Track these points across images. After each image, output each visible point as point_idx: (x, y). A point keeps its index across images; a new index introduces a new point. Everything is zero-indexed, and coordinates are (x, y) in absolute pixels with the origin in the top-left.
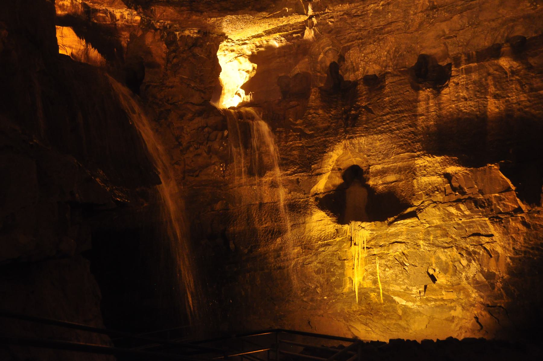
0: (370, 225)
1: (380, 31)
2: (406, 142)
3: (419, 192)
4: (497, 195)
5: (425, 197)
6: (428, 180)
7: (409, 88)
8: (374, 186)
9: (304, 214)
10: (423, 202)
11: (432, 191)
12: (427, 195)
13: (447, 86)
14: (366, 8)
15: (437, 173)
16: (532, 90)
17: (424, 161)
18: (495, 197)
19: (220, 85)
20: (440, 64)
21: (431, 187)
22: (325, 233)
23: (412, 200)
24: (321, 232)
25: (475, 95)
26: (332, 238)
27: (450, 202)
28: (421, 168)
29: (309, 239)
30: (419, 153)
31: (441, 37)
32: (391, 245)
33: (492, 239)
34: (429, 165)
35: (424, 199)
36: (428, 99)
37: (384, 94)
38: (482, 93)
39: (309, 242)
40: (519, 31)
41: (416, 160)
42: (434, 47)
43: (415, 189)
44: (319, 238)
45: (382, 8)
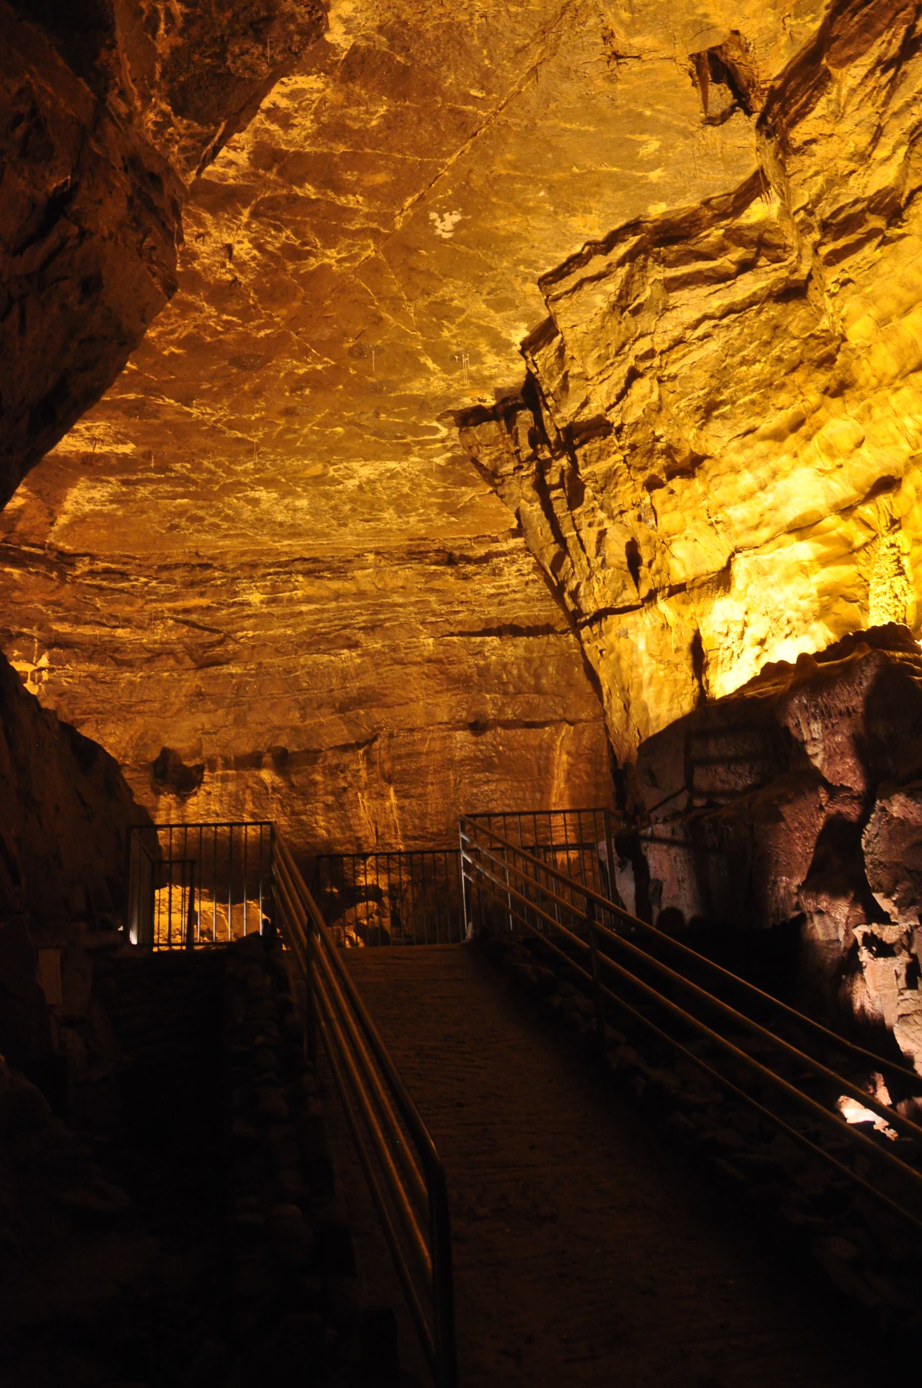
1: (128, 708)
7: (148, 790)
13: (195, 794)
14: (119, 676)
16: (293, 813)
19: (874, 1021)
20: (185, 763)
25: (230, 811)
36: (169, 808)
38: (238, 809)
40: (283, 741)
42: (181, 741)
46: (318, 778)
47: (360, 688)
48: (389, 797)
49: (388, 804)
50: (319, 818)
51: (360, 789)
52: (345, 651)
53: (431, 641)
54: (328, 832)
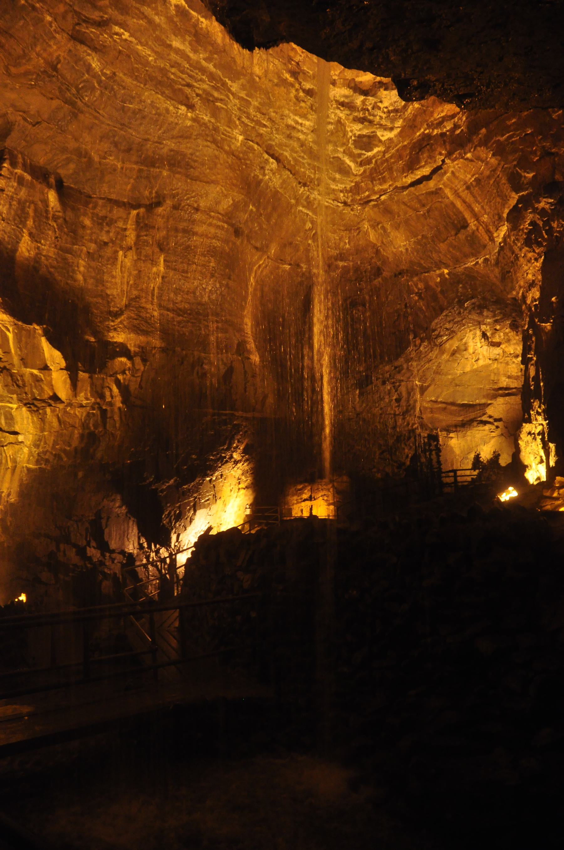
4: (35, 372)
18: (32, 374)
33: (17, 439)
46: (87, 222)
47: (171, 150)
49: (154, 269)
50: (82, 262)
51: (122, 248)
52: (183, 108)
53: (241, 138)
54: (85, 280)
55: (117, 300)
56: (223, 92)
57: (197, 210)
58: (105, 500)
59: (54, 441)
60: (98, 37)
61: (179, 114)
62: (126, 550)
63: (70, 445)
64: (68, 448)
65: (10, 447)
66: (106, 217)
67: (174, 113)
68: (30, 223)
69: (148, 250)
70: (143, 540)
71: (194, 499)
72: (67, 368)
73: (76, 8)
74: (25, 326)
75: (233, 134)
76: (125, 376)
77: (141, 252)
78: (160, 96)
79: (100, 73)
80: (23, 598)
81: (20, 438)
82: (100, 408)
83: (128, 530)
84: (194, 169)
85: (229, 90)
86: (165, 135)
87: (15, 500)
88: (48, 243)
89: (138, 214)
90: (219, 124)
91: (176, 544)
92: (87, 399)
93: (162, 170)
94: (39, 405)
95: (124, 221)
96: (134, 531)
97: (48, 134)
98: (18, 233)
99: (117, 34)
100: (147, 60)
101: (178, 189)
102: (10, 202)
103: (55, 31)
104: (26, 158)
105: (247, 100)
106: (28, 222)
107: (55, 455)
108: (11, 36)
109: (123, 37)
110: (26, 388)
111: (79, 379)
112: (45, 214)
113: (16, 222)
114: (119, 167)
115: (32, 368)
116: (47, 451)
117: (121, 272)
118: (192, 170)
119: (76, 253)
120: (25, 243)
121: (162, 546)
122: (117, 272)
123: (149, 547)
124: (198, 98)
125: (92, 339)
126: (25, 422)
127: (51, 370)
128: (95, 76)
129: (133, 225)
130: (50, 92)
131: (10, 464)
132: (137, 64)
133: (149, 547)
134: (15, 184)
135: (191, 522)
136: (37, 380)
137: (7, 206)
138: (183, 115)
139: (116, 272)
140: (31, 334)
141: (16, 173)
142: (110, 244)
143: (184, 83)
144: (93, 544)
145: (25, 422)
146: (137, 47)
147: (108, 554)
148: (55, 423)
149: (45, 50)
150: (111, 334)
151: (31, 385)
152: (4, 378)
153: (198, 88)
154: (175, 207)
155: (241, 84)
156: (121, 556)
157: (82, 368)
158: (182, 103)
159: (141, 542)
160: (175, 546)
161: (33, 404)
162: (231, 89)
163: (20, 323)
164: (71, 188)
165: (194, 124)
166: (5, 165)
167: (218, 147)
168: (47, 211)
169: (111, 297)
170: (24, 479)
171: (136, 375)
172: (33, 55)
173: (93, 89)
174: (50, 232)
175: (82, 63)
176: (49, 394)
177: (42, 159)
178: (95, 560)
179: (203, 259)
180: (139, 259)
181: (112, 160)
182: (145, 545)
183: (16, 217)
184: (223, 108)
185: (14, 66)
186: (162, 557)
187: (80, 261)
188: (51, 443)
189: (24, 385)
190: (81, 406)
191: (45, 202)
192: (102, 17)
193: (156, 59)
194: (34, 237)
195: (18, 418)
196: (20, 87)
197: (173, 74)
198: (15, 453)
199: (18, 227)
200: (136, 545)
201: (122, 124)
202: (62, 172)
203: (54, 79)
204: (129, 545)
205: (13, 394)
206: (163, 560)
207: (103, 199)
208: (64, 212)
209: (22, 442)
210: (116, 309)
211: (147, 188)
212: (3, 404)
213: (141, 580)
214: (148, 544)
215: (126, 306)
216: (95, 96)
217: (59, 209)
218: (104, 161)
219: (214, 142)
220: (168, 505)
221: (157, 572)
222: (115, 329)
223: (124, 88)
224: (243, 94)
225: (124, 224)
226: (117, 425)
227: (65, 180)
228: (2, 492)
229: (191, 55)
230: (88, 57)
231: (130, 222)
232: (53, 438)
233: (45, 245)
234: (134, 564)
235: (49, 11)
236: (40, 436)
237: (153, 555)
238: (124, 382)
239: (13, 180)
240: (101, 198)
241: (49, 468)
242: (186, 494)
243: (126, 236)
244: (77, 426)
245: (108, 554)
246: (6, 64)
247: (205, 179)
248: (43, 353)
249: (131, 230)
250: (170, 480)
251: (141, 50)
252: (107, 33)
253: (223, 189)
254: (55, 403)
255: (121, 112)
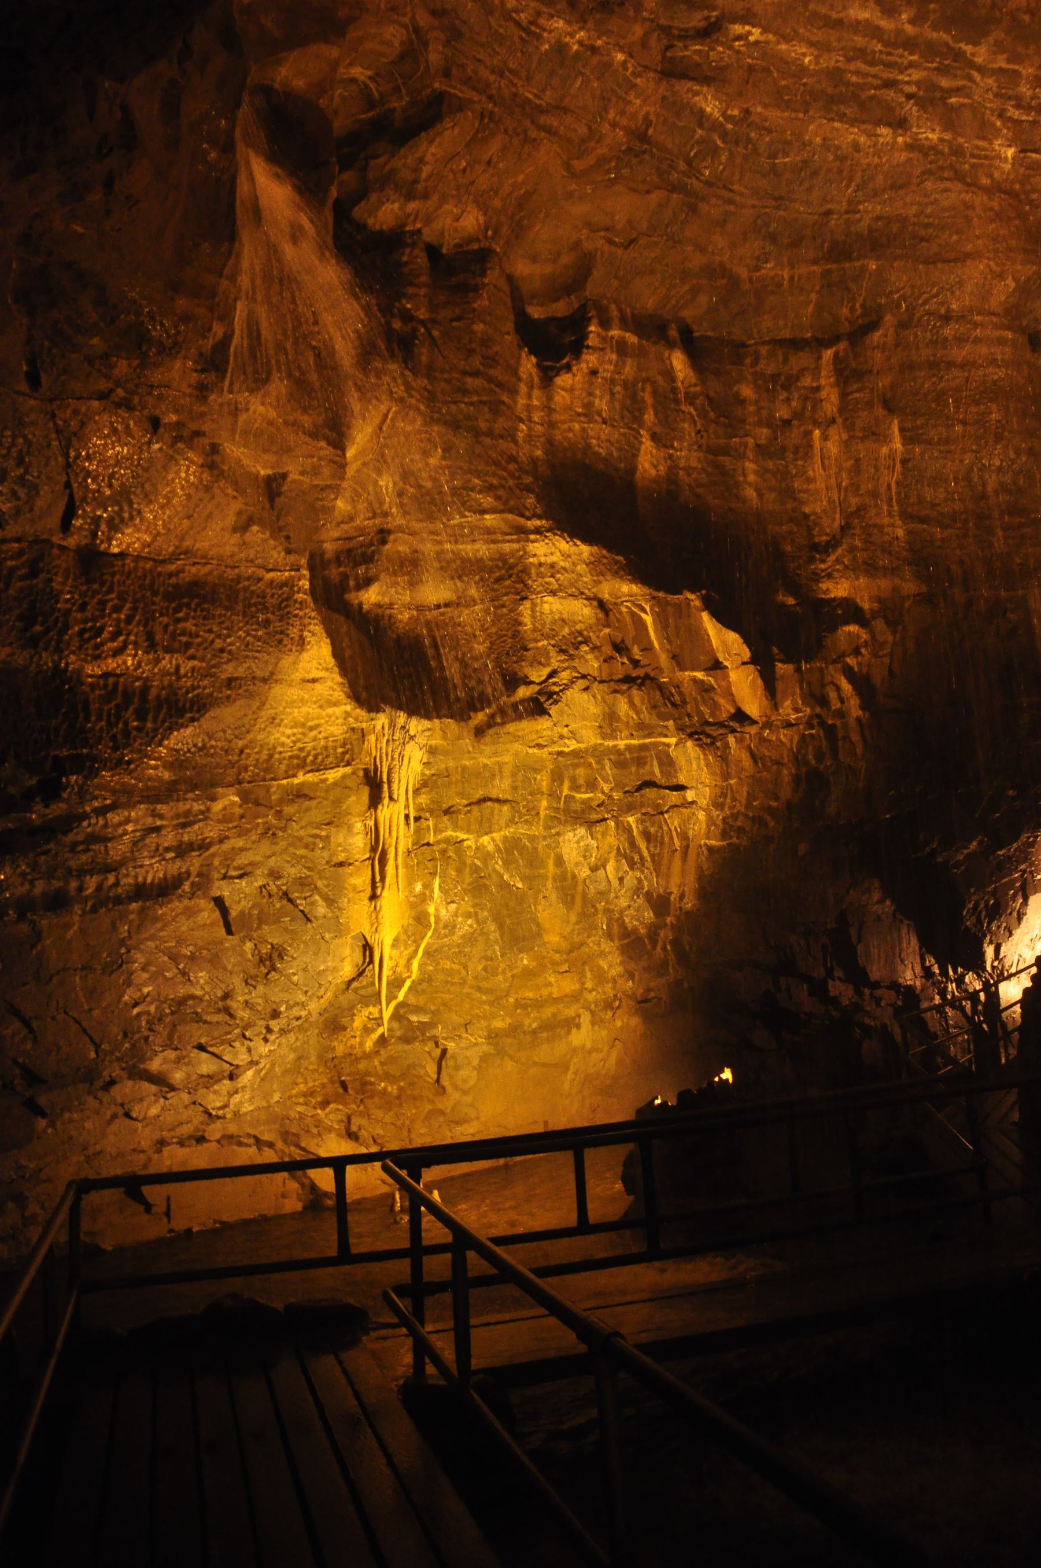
0: (429, 730)
2: (503, 482)
3: (539, 641)
4: (700, 675)
5: (559, 658)
6: (560, 607)
8: (380, 611)
9: (278, 637)
10: (553, 674)
11: (573, 644)
12: (562, 651)
13: (568, 368)
15: (582, 593)
17: (553, 549)
18: (694, 680)
21: (566, 630)
22: (315, 739)
23: (523, 663)
24: (303, 734)
26: (342, 760)
27: (612, 680)
28: (542, 569)
29: (264, 756)
30: (538, 523)
31: (598, 230)
32: (475, 808)
33: (684, 798)
34: (562, 564)
35: (555, 663)
37: (475, 310)
39: (266, 770)
41: (533, 542)
43: (525, 632)
44: (298, 757)
45: (577, 51)
46: (747, 391)
48: (887, 439)
49: (885, 450)
50: (750, 466)
51: (817, 424)
52: (883, 130)
54: (760, 496)
55: (825, 522)
56: (959, 72)
57: (947, 318)
58: (851, 892)
59: (748, 793)
60: (708, 56)
61: (879, 146)
62: (901, 981)
63: (777, 798)
64: (774, 804)
65: (673, 813)
66: (779, 375)
67: (869, 147)
68: (649, 416)
69: (863, 418)
70: (930, 961)
71: (1022, 876)
72: (754, 661)
73: (663, 22)
74: (670, 597)
75: (994, 150)
76: (860, 658)
77: (853, 424)
78: (837, 125)
79: (721, 119)
80: (727, 1075)
81: (690, 795)
82: (822, 724)
83: (900, 942)
84: (928, 241)
85: (972, 65)
86: (860, 193)
87: (693, 905)
88: (685, 444)
89: (836, 355)
90: (961, 140)
91: (996, 964)
92: (797, 710)
93: (865, 262)
94: (714, 734)
95: (813, 375)
96: (911, 944)
97: (653, 255)
98: (632, 439)
99: (739, 38)
100: (802, 65)
101: (903, 288)
102: (611, 390)
103: (633, 73)
104: (623, 306)
105: (1014, 71)
106: (646, 416)
107: (753, 819)
108: (566, 110)
109: (751, 39)
110: (689, 706)
111: (777, 676)
112: (671, 396)
113: (626, 421)
114: (786, 277)
115: (693, 670)
116: (739, 812)
117: (824, 468)
118: (924, 244)
119: (736, 450)
120: (646, 452)
121: (968, 969)
122: (816, 470)
123: (944, 973)
124: (912, 102)
125: (791, 601)
126: (694, 766)
127: (726, 667)
128: (716, 127)
129: (830, 377)
130: (643, 182)
131: (677, 843)
132: (785, 79)
133: (944, 973)
134: (614, 357)
135: (1019, 919)
136: (705, 689)
137: (608, 397)
138: (887, 143)
139: (814, 470)
140: (683, 611)
141: (612, 338)
142: (795, 422)
143: (879, 82)
144: (839, 973)
145: (694, 766)
146: (779, 47)
147: (867, 991)
148: (747, 762)
149: (622, 113)
150: (823, 586)
151: (695, 699)
152: (648, 694)
153: (908, 83)
154: (903, 325)
155: (992, 42)
156: (892, 993)
157: (782, 657)
158: (879, 123)
159: (927, 964)
160: (993, 967)
161: (703, 733)
162: (976, 59)
163: (661, 594)
164: (708, 338)
165: (911, 155)
166: (592, 328)
167: (968, 185)
168: (674, 390)
169: (812, 518)
170: (705, 867)
171: (881, 653)
172: (606, 128)
173: (715, 151)
174: (686, 425)
175: (687, 112)
176: (728, 711)
177: (650, 302)
178: (845, 1002)
179: (974, 409)
180: (852, 437)
181: (772, 269)
182: (936, 970)
183: (625, 413)
184: (963, 105)
185: (578, 158)
186: (971, 990)
187: (747, 464)
188: (743, 796)
189: (684, 702)
190: (789, 725)
191: (669, 374)
192: (708, 18)
193: (817, 58)
194: (660, 440)
195: (681, 762)
196: (593, 190)
197: (854, 73)
198: (685, 822)
199: (630, 428)
200: (918, 969)
201: (776, 199)
202: (688, 314)
203: (647, 157)
204: (904, 972)
205: (667, 720)
206: (974, 996)
207: (769, 343)
208: (703, 383)
209: (693, 802)
210: (824, 538)
211: (845, 302)
212: (653, 740)
213: (935, 1036)
214: (939, 968)
215: (842, 529)
216: (720, 163)
217: (694, 381)
218: (758, 274)
219: (959, 176)
220: (972, 890)
221: (963, 1019)
222: (829, 576)
223: (769, 131)
224: (1001, 63)
225: (813, 380)
226: (859, 751)
227: (694, 327)
228: (671, 893)
229: (884, 23)
230: (697, 98)
231: (823, 373)
232: (745, 789)
233: (681, 450)
234: (918, 1007)
235: (618, 44)
236: (722, 788)
237: (952, 987)
238: (860, 670)
239: (608, 350)
240: (764, 343)
241: (745, 843)
242: (1004, 867)
243: (822, 401)
244: (786, 760)
245: (867, 991)
246: (565, 158)
247: (952, 255)
248: (709, 641)
249: (827, 388)
250: (971, 843)
251: (789, 51)
252: (722, 44)
253: (992, 264)
254: (742, 726)
255: (772, 176)
